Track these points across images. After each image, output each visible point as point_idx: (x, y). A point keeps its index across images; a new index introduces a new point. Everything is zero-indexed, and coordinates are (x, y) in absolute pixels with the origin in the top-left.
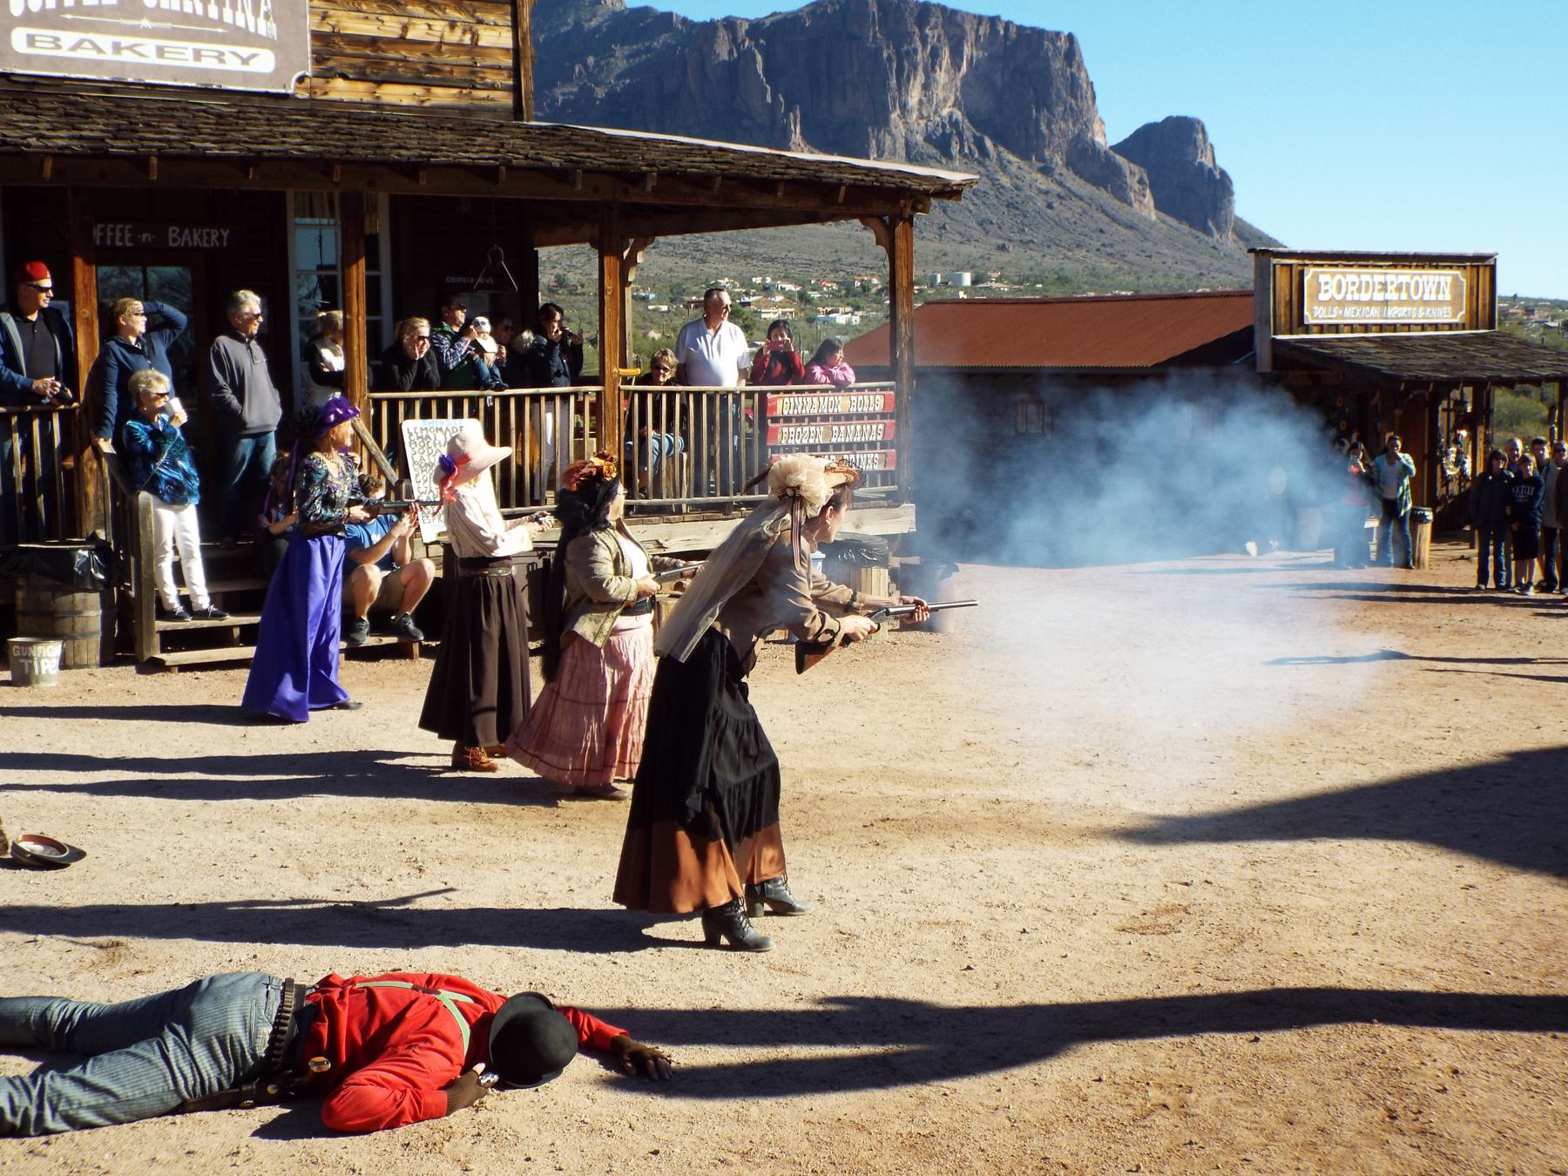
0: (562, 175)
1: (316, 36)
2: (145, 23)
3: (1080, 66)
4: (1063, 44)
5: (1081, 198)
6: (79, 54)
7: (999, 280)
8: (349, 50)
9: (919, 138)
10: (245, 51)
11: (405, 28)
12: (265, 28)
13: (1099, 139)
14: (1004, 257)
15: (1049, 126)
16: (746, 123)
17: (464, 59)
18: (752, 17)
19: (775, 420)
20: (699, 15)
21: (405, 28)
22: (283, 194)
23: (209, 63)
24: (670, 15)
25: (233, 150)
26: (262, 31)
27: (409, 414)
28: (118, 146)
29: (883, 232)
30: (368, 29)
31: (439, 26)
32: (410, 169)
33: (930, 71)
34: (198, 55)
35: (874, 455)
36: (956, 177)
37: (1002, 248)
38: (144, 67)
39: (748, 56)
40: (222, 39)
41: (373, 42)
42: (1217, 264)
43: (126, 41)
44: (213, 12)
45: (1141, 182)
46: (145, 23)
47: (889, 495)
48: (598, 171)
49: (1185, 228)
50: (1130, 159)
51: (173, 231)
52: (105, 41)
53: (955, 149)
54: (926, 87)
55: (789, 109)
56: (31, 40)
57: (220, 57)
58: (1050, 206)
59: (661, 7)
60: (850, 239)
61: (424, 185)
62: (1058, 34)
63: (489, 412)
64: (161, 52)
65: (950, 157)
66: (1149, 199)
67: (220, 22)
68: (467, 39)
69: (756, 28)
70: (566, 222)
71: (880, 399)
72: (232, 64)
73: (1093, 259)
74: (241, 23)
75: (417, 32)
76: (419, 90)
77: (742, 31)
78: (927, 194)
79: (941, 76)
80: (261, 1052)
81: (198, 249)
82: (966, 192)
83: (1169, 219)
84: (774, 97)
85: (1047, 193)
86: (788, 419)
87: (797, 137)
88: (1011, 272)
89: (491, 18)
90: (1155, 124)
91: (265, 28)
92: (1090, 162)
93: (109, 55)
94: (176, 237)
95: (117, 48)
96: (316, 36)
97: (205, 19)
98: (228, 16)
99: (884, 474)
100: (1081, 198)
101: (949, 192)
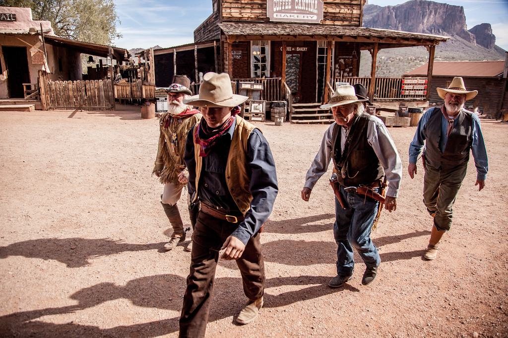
0: (368, 37)
1: (324, 12)
2: (295, 11)
3: (463, 13)
4: (460, 9)
5: (459, 41)
6: (285, 17)
7: (440, 58)
8: (330, 15)
9: (425, 29)
10: (312, 16)
11: (340, 11)
12: (316, 11)
13: (465, 29)
14: (441, 53)
15: (454, 26)
16: (390, 26)
17: (350, 16)
18: (393, 5)
19: (403, 84)
20: (383, 6)
21: (340, 11)
22: (316, 42)
23: (306, 18)
24: (377, 6)
25: (311, 34)
26: (315, 12)
27: (337, 81)
28: (291, 33)
29: (428, 48)
30: (333, 11)
31: (346, 10)
32: (341, 37)
33: (430, 15)
34: (304, 17)
35: (422, 92)
36: (445, 37)
37: (441, 51)
38: (294, 19)
39: (391, 13)
40: (308, 14)
41: (334, 13)
42: (489, 55)
43: (292, 15)
44: (307, 9)
45: (474, 37)
46: (295, 11)
47: (424, 99)
48: (375, 37)
49: (483, 47)
50: (472, 33)
51: (298, 48)
52: (289, 15)
53: (433, 31)
54: (428, 19)
55: (399, 23)
56: (277, 15)
57: (308, 17)
58: (452, 43)
59: (375, 4)
60: (422, 51)
61: (343, 40)
62: (459, 7)
63: (264, 83)
64: (298, 17)
65: (439, 32)
66: (475, 41)
67: (308, 11)
68: (351, 12)
69: (394, 8)
70: (366, 46)
71: (424, 81)
72: (310, 18)
73: (460, 54)
74: (311, 11)
75: (342, 11)
76: (342, 22)
77: (391, 9)
78: (439, 41)
79: (432, 16)
80: (184, 188)
81: (302, 51)
82: (447, 40)
83: (479, 45)
84: (396, 21)
85: (452, 40)
86: (406, 84)
87: (400, 28)
88: (442, 56)
89: (355, 8)
90: (479, 25)
91: (316, 11)
92: (464, 35)
93: (289, 18)
94: (298, 49)
95: (290, 16)
96: (324, 12)
97: (305, 10)
98: (309, 10)
99: (424, 95)
100: (459, 41)
101: (444, 40)
